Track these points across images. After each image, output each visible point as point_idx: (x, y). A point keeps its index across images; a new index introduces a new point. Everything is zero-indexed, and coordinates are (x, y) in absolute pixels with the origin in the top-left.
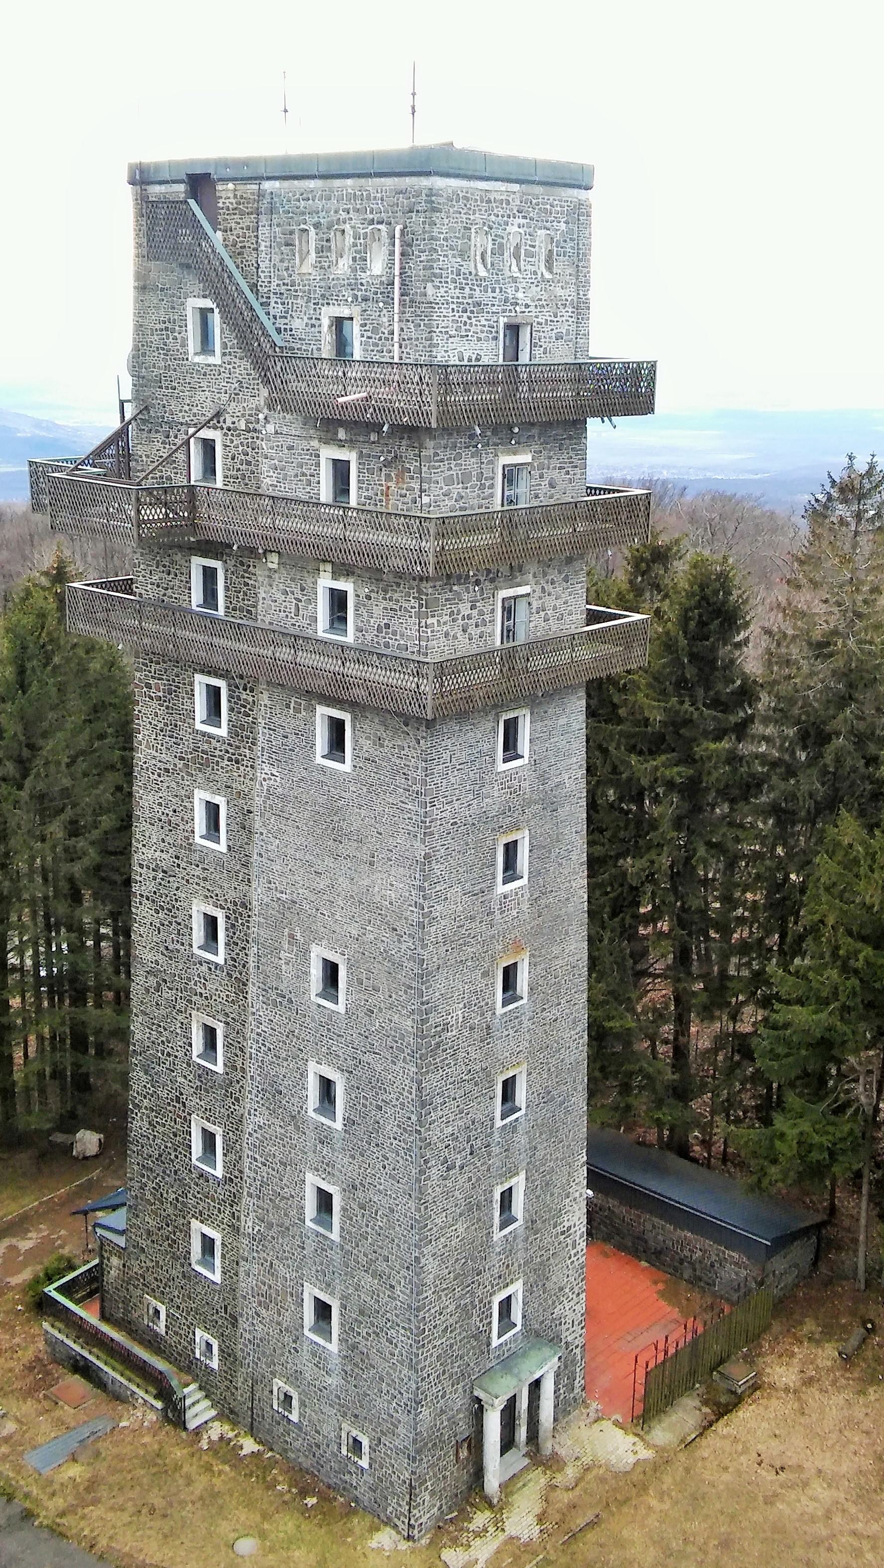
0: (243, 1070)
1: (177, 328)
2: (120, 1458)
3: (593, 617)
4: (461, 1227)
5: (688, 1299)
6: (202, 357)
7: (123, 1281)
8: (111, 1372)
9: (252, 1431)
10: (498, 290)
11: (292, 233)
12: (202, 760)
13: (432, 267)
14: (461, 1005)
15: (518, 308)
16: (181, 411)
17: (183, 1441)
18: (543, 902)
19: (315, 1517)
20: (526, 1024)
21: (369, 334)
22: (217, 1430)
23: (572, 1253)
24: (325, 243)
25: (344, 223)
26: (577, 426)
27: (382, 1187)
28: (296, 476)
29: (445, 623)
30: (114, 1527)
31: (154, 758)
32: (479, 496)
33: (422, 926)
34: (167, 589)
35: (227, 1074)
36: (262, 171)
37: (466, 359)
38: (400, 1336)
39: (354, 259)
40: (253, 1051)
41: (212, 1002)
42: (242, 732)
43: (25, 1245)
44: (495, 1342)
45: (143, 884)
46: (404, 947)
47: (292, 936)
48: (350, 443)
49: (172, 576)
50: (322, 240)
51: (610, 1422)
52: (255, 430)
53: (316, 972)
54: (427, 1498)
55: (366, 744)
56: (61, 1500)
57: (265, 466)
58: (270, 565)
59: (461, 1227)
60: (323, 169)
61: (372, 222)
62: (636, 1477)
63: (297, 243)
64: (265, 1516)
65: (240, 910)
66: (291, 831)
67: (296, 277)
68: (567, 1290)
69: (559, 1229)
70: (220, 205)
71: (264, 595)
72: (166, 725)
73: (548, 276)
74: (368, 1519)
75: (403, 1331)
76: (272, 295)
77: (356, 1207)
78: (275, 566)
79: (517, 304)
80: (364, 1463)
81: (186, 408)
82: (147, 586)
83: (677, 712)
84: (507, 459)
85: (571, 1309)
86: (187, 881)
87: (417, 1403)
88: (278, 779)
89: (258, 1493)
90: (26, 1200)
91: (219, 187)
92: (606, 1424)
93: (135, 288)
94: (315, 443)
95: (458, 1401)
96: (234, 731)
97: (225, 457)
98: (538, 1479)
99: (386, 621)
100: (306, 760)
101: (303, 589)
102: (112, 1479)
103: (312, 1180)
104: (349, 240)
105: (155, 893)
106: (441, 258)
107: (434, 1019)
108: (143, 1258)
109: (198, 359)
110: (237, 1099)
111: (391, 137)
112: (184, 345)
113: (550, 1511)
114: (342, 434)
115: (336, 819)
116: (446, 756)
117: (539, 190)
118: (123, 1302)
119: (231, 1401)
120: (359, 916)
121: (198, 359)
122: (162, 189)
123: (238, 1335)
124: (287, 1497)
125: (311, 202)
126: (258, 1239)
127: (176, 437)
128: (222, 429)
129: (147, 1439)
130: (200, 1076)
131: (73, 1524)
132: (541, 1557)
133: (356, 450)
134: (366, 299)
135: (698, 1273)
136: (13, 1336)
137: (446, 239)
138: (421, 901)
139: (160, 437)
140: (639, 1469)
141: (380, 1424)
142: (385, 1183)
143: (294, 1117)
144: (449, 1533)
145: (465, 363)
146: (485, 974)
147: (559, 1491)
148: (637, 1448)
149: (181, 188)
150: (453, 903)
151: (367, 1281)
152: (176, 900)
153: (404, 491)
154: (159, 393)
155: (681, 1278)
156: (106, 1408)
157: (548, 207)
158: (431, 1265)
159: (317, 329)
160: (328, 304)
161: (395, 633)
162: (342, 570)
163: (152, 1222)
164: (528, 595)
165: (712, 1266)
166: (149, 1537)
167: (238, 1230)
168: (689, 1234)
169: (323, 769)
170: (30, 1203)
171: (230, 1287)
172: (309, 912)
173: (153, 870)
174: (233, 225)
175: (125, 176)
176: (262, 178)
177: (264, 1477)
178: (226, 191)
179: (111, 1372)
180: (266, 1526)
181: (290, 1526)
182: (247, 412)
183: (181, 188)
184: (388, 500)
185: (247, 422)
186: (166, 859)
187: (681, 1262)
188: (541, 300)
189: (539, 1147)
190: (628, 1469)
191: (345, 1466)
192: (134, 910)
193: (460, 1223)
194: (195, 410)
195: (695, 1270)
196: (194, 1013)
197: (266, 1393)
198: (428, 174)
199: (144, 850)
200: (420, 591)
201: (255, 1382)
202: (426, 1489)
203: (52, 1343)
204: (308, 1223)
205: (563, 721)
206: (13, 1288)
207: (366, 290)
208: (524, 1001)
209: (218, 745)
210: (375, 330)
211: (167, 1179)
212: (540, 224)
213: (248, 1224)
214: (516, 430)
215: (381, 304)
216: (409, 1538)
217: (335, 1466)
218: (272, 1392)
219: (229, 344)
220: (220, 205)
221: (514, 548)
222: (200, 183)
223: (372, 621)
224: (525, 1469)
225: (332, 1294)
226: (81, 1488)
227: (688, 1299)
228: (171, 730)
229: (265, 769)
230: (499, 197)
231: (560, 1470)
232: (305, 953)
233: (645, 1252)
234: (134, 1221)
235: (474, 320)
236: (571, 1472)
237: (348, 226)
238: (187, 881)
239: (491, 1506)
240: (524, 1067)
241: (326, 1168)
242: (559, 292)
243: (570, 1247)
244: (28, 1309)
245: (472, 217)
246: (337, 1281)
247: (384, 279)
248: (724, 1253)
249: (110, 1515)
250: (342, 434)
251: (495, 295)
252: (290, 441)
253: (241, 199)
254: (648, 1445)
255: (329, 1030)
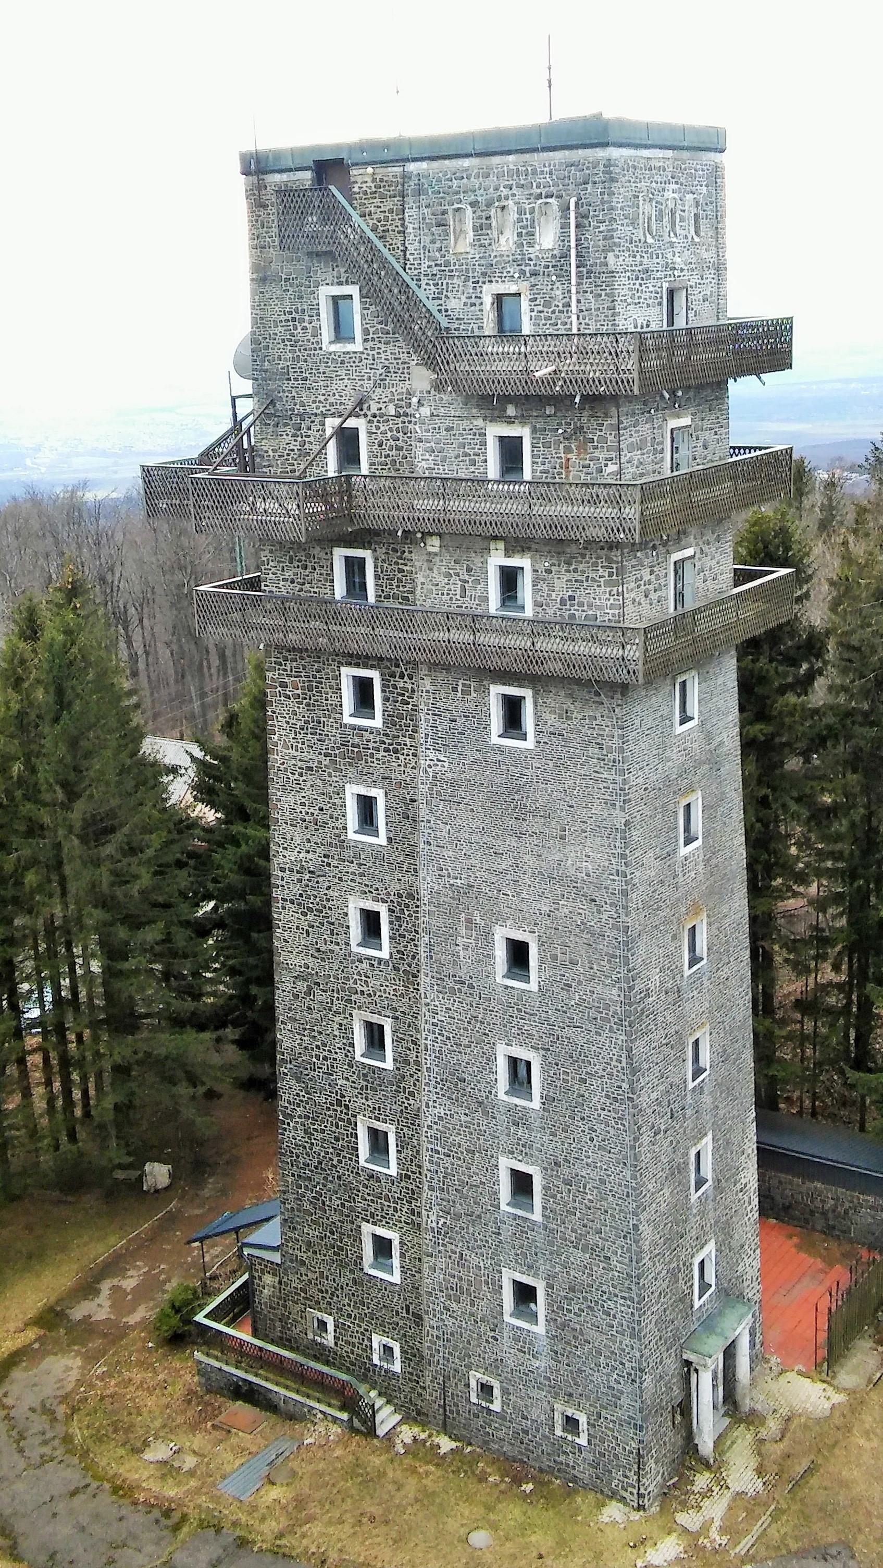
0: (417, 1063)
1: (307, 318)
2: (318, 1474)
3: (741, 577)
4: (667, 1192)
5: (825, 1249)
6: (339, 345)
7: (280, 1298)
8: (281, 1391)
9: (445, 1428)
10: (660, 256)
11: (444, 213)
12: (353, 753)
13: (612, 237)
14: (658, 970)
15: (676, 272)
16: (314, 402)
17: (377, 1449)
18: (714, 861)
19: (538, 1501)
20: (706, 983)
21: (540, 308)
22: (407, 1433)
23: (749, 1209)
24: (484, 221)
25: (507, 198)
26: (721, 387)
27: (590, 1161)
28: (457, 457)
29: (632, 590)
30: (340, 1540)
31: (294, 757)
32: (653, 461)
33: (625, 893)
34: (304, 584)
35: (398, 1069)
36: (406, 153)
37: (639, 326)
38: (619, 1307)
39: (520, 235)
40: (428, 1042)
41: (376, 998)
42: (401, 721)
43: (129, 1283)
44: (697, 1304)
45: (285, 887)
46: (605, 916)
47: (469, 921)
48: (522, 419)
49: (310, 569)
50: (480, 218)
51: (794, 1373)
52: (406, 415)
53: (501, 953)
54: (653, 1465)
55: (551, 719)
56: (274, 1524)
57: (419, 450)
58: (430, 549)
59: (667, 1192)
60: (479, 147)
61: (540, 196)
62: (838, 1420)
63: (452, 223)
64: (489, 1508)
65: (406, 904)
66: (466, 815)
67: (451, 258)
68: (746, 1247)
69: (739, 1186)
70: (356, 189)
71: (423, 580)
72: (307, 722)
73: (697, 239)
74: (591, 1496)
75: (622, 1301)
76: (422, 278)
77: (560, 1183)
78: (436, 549)
79: (675, 269)
80: (583, 1440)
81: (322, 398)
82: (279, 581)
83: (752, 672)
84: (673, 423)
85: (751, 1265)
86: (340, 879)
87: (642, 1370)
88: (446, 764)
89: (473, 1486)
90: (112, 1240)
91: (354, 172)
92: (791, 1376)
93: (252, 280)
94: (479, 422)
95: (672, 1365)
96: (390, 719)
97: (370, 444)
98: (744, 1438)
99: (570, 593)
100: (470, 741)
101: (469, 570)
102: (318, 1495)
103: (505, 1163)
104: (513, 215)
105: (301, 895)
106: (620, 228)
107: (639, 986)
108: (303, 1270)
109: (333, 348)
110: (411, 1094)
111: (525, 112)
112: (316, 332)
113: (765, 1463)
114: (511, 411)
115: (517, 797)
116: (637, 722)
117: (686, 155)
118: (281, 1320)
119: (419, 1403)
120: (551, 892)
121: (333, 348)
122: (284, 177)
123: (424, 1333)
124: (503, 1486)
125: (465, 180)
126: (444, 1233)
127: (309, 429)
128: (365, 416)
129: (338, 1452)
130: (365, 1075)
131: (296, 1544)
132: (773, 1507)
133: (530, 425)
134: (534, 274)
135: (831, 1223)
136: (156, 1373)
137: (622, 209)
138: (624, 868)
139: (290, 430)
140: (837, 1414)
141: (598, 1399)
142: (594, 1156)
143: (480, 1103)
144: (676, 1497)
145: (639, 330)
146: (674, 937)
147: (768, 1445)
148: (829, 1394)
149: (308, 175)
150: (648, 869)
151: (578, 1256)
152: (328, 900)
153: (588, 462)
154: (286, 385)
155: (813, 1229)
156: (286, 1428)
157: (693, 171)
158: (646, 1230)
159: (478, 308)
160: (490, 282)
161: (581, 604)
162: (516, 545)
163: (313, 1233)
164: (693, 557)
165: (846, 1212)
166: (379, 1544)
167: (419, 1225)
168: (819, 1185)
169: (500, 749)
170: (116, 1242)
171: (411, 1286)
172: (490, 894)
173: (298, 872)
174: (373, 209)
175: (238, 167)
176: (407, 160)
177: (473, 1473)
178: (362, 177)
179: (281, 1391)
180: (492, 1517)
181: (517, 1512)
182: (396, 398)
183: (308, 175)
184: (568, 472)
185: (397, 406)
186: (313, 859)
187: (812, 1213)
188: (691, 263)
189: (720, 1106)
190: (827, 1413)
191: (559, 1446)
192: (275, 916)
193: (666, 1187)
194: (331, 399)
195: (827, 1219)
196: (355, 1012)
197: (461, 1387)
198: (606, 145)
199: (285, 853)
200: (609, 560)
201: (447, 1378)
202: (652, 1456)
203: (203, 1371)
204: (504, 1207)
205: (720, 680)
206: (133, 1328)
207: (535, 265)
208: (704, 962)
209: (372, 736)
210: (547, 304)
211: (330, 1186)
212: (688, 189)
213: (431, 1219)
214: (680, 393)
215: (554, 278)
216: (640, 1508)
217: (547, 1449)
218: (468, 1385)
219: (371, 330)
220: (356, 189)
221: (677, 510)
222: (329, 169)
223: (554, 594)
224: (729, 1428)
225: (535, 1275)
226: (290, 1509)
227: (825, 1249)
228: (315, 727)
229: (428, 757)
230: (658, 164)
231: (763, 1424)
232: (488, 936)
233: (772, 1209)
234: (289, 1234)
235: (644, 286)
236: (773, 1426)
237: (510, 202)
238: (340, 879)
239: (708, 1466)
240: (707, 1028)
241: (522, 1149)
242: (705, 255)
243: (746, 1204)
244: (159, 1345)
245: (639, 185)
246: (541, 1262)
247: (555, 252)
248: (858, 1198)
249: (331, 1530)
250: (511, 411)
251: (658, 261)
252: (448, 423)
253: (380, 183)
254: (837, 1389)
255: (519, 1010)
